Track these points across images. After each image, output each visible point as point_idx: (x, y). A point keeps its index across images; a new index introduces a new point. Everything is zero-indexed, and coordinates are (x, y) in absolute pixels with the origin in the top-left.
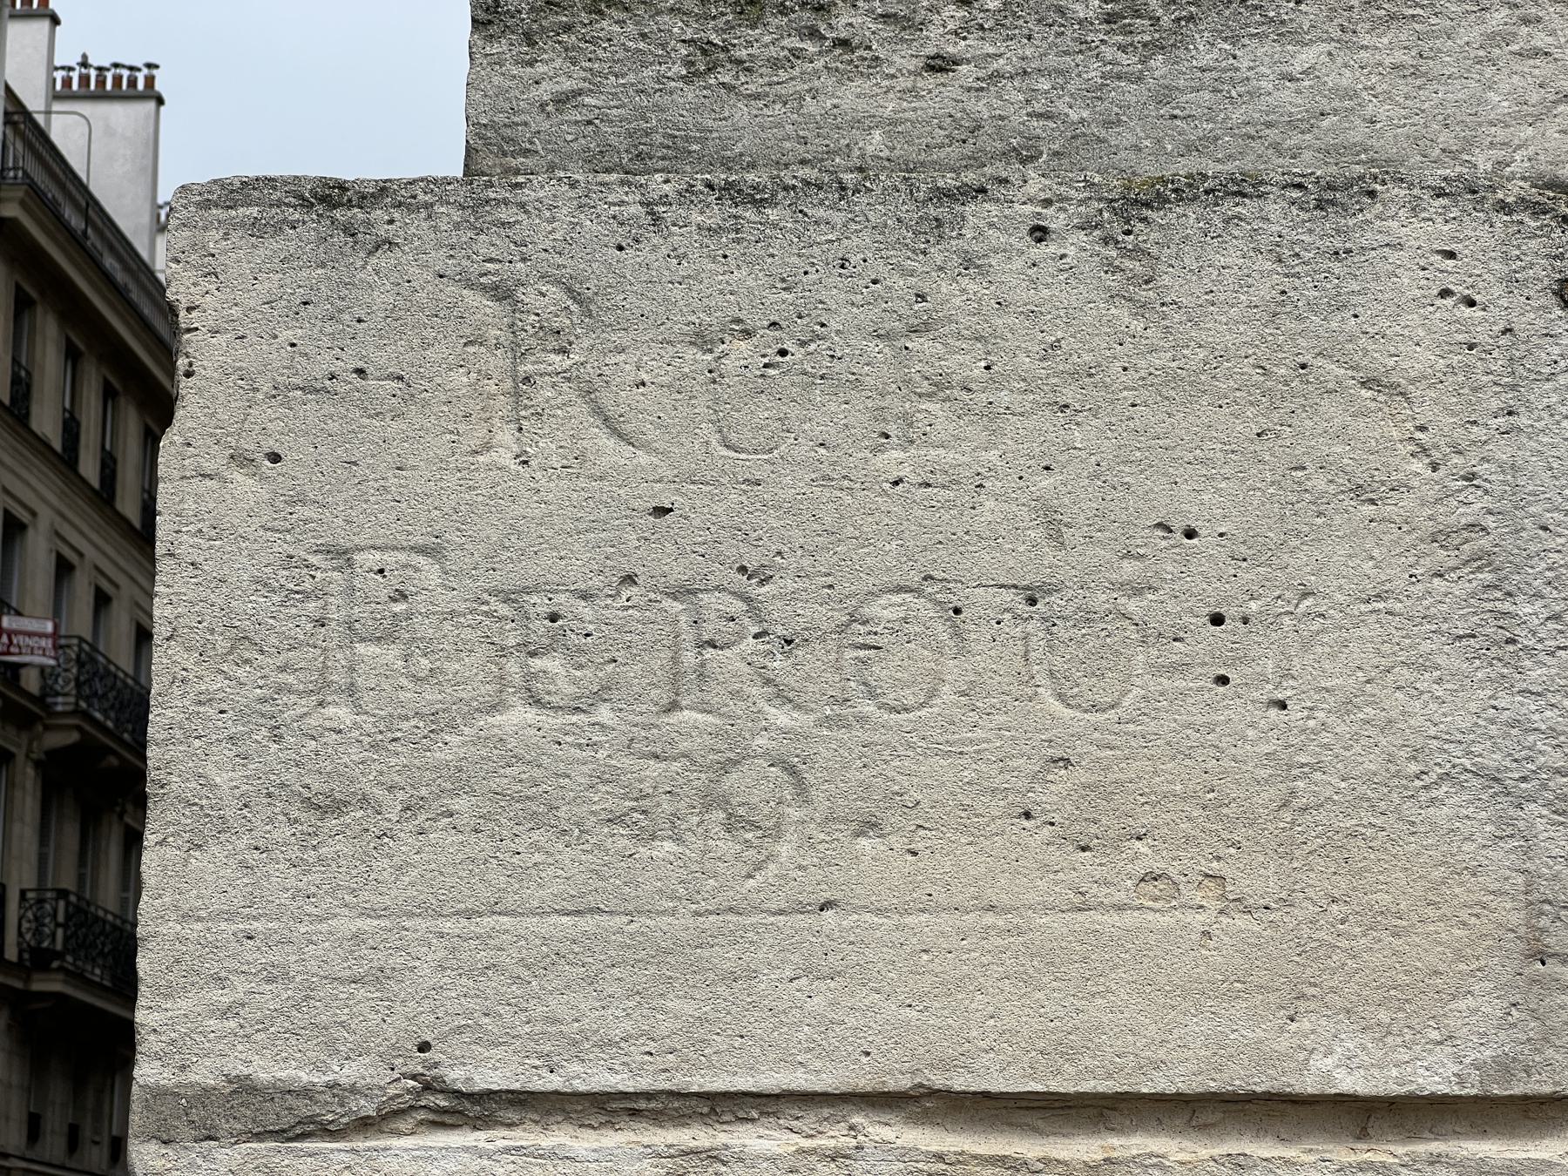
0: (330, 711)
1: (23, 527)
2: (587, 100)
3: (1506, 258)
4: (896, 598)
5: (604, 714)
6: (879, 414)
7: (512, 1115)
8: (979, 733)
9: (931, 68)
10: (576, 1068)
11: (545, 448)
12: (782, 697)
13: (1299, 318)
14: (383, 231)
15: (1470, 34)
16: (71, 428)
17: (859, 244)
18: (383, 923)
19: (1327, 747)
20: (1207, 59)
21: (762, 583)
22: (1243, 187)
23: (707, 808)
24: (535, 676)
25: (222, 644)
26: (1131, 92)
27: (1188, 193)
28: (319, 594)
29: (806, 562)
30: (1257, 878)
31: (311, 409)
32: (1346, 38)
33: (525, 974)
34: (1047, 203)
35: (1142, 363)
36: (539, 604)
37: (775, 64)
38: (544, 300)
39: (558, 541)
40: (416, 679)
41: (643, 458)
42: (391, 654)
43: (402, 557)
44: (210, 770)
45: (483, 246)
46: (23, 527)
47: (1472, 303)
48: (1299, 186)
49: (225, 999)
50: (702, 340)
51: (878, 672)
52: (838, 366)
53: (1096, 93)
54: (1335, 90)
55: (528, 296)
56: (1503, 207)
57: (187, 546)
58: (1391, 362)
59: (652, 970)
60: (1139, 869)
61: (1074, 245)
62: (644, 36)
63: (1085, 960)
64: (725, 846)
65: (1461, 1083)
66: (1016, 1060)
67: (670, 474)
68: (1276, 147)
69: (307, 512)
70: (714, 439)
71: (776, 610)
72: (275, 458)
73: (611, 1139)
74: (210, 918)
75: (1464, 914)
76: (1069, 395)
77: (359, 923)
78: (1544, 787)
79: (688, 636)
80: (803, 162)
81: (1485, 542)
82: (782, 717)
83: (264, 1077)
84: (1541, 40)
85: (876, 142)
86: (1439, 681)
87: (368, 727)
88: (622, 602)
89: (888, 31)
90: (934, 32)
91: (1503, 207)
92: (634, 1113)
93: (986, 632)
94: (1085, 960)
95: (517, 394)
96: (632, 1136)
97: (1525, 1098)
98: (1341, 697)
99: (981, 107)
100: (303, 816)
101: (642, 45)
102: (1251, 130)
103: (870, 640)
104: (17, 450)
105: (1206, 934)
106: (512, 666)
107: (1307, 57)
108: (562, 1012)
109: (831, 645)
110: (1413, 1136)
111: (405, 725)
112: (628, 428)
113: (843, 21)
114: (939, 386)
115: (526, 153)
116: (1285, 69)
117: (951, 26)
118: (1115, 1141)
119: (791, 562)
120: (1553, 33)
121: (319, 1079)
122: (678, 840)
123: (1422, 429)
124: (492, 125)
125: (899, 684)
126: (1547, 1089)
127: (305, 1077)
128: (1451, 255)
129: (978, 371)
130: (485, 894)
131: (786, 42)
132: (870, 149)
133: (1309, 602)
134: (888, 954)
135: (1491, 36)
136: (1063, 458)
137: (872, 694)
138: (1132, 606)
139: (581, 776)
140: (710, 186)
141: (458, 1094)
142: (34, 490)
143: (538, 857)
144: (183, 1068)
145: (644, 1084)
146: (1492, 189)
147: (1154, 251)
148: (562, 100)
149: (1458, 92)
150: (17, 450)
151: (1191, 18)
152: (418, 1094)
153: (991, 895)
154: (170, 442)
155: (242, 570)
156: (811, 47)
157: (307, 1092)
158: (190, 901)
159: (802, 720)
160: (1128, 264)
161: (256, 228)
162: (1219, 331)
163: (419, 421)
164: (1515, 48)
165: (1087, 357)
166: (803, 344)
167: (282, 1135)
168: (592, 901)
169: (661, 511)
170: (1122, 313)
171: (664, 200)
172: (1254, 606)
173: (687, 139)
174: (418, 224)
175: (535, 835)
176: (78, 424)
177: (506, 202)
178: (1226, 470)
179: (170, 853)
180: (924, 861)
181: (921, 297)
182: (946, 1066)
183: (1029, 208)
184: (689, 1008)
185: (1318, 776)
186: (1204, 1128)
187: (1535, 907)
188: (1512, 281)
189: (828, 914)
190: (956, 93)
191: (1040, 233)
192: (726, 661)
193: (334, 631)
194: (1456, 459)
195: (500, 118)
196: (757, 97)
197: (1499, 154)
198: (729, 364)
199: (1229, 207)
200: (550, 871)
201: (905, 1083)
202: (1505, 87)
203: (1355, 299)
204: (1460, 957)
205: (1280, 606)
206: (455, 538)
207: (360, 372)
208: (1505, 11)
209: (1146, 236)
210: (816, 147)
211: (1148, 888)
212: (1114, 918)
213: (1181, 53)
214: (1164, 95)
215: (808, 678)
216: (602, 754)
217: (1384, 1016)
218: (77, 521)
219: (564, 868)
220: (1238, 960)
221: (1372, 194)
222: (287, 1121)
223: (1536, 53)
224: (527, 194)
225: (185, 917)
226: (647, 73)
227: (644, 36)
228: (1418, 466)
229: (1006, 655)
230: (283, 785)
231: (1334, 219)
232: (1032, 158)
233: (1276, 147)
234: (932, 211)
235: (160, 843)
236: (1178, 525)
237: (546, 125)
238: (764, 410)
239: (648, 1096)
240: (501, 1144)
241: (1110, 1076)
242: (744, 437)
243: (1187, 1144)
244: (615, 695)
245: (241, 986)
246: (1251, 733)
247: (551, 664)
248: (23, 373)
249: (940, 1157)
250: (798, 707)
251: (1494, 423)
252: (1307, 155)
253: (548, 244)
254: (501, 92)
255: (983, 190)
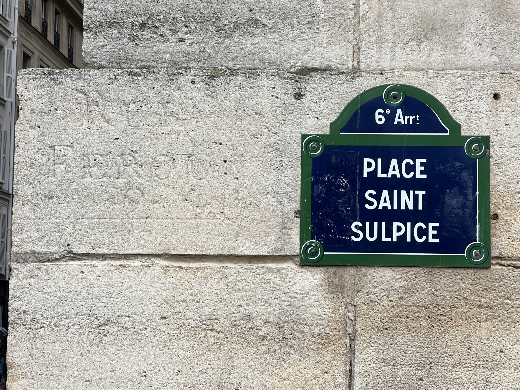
0: (50, 178)
1: (30, 57)
2: (108, 47)
3: (285, 89)
4: (162, 157)
5: (105, 179)
6: (160, 119)
7: (86, 258)
8: (178, 184)
9: (180, 41)
10: (98, 249)
11: (94, 126)
12: (139, 176)
13: (244, 100)
14: (61, 80)
15: (291, 35)
16: (44, 25)
17: (157, 84)
18: (61, 220)
19: (245, 187)
20: (237, 40)
21: (136, 153)
22: (234, 72)
23: (125, 198)
24: (91, 171)
25: (28, 165)
26: (221, 47)
27: (223, 74)
28: (48, 154)
29: (145, 149)
30: (231, 213)
31: (46, 117)
32: (265, 36)
33: (88, 231)
34: (195, 76)
35: (212, 109)
36: (92, 157)
37: (147, 39)
38: (93, 95)
39: (96, 145)
40: (68, 172)
41: (113, 128)
42: (63, 167)
43: (65, 147)
44: (26, 190)
45: (82, 83)
46: (30, 57)
47: (278, 98)
48: (245, 73)
49: (29, 235)
50: (125, 104)
51: (158, 171)
52: (152, 110)
53: (214, 47)
54: (262, 47)
55: (90, 94)
56: (285, 78)
57: (21, 145)
58: (261, 110)
59: (113, 230)
60: (208, 211)
61: (200, 85)
62: (120, 33)
63: (197, 229)
64: (128, 206)
65: (268, 253)
66: (183, 248)
67: (118, 131)
68: (250, 59)
69: (45, 138)
70: (127, 124)
71: (139, 159)
72: (39, 127)
73: (105, 263)
74: (26, 219)
75: (270, 220)
76: (198, 116)
77: (56, 220)
78: (287, 195)
79: (122, 164)
80: (153, 61)
81: (278, 146)
82: (139, 180)
83: (37, 250)
84: (305, 37)
85: (168, 57)
86: (268, 174)
87: (58, 182)
88: (108, 157)
89: (171, 33)
90: (180, 33)
91: (285, 78)
92: (110, 258)
93: (180, 163)
94: (197, 229)
95: (88, 115)
96: (109, 262)
97: (280, 255)
98: (249, 177)
99: (190, 49)
100: (45, 199)
101: (119, 35)
102: (245, 55)
103: (157, 165)
104: (27, 32)
105: (220, 224)
106: (87, 170)
107: (257, 40)
108: (96, 238)
109: (149, 166)
110: (260, 263)
111: (65, 181)
112: (110, 122)
113: (162, 30)
114: (172, 114)
115: (95, 58)
116: (252, 42)
117: (184, 32)
118: (202, 264)
119: (142, 149)
120: (308, 35)
121: (48, 251)
122: (119, 204)
123: (267, 123)
124: (88, 52)
125: (162, 174)
126: (284, 254)
127: (45, 250)
128: (274, 88)
129: (180, 111)
130: (81, 215)
131: (149, 35)
132: (167, 58)
133: (243, 158)
134: (159, 227)
135: (295, 36)
136: (196, 128)
137: (157, 176)
138: (209, 158)
139: (100, 191)
140: (127, 72)
141: (75, 254)
142: (33, 45)
143: (91, 208)
144: (21, 248)
145: (111, 252)
146: (283, 74)
147: (216, 86)
148: (102, 47)
149: (287, 48)
150: (27, 32)
151: (234, 31)
152: (67, 254)
153: (179, 216)
154: (18, 122)
155: (32, 149)
156: (155, 36)
157: (45, 253)
158: (22, 215)
159: (143, 181)
160: (211, 89)
161: (35, 79)
162: (228, 103)
163: (68, 120)
164: (300, 39)
165: (201, 108)
166: (145, 105)
167: (40, 261)
168: (102, 216)
169: (117, 139)
170: (209, 99)
171: (118, 75)
172: (232, 159)
173: (129, 55)
174: (68, 79)
175: (91, 203)
176: (47, 23)
177: (86, 74)
178: (228, 131)
179: (18, 206)
180: (166, 209)
181: (169, 95)
182: (169, 249)
183: (191, 77)
184: (120, 237)
185: (244, 193)
186: (220, 261)
187: (284, 219)
188: (286, 94)
189: (147, 219)
190: (185, 46)
191: (193, 82)
192: (129, 169)
193: (51, 162)
194: (273, 129)
195: (89, 50)
196: (143, 47)
197: (295, 61)
198: (130, 109)
199: (231, 77)
200: (94, 210)
201: (162, 252)
202: (297, 47)
203: (255, 97)
204: (269, 229)
205: (238, 159)
206: (75, 143)
207: (56, 109)
208: (298, 31)
209: (214, 83)
210: (156, 57)
211: (209, 215)
212: (203, 221)
213: (231, 39)
214: (228, 48)
215: (145, 172)
216: (104, 187)
217: (254, 240)
218: (47, 55)
219: (96, 210)
220: (226, 229)
221: (259, 75)
222: (42, 259)
223: (304, 40)
224: (90, 73)
225: (21, 219)
226: (120, 41)
227: (120, 33)
228: (266, 130)
229: (183, 168)
230: (40, 193)
231: (252, 80)
232: (200, 61)
233: (250, 59)
234: (172, 77)
235: (16, 204)
236: (218, 142)
237: (99, 52)
238: (137, 118)
239: (112, 254)
240: (83, 263)
241: (201, 251)
242: (133, 124)
243: (216, 264)
244: (107, 175)
245: (32, 232)
246: (231, 184)
247: (95, 169)
248: (29, 7)
249: (168, 267)
250: (142, 178)
251: (281, 122)
252: (256, 61)
253: (94, 83)
254: (90, 45)
255: (182, 73)
